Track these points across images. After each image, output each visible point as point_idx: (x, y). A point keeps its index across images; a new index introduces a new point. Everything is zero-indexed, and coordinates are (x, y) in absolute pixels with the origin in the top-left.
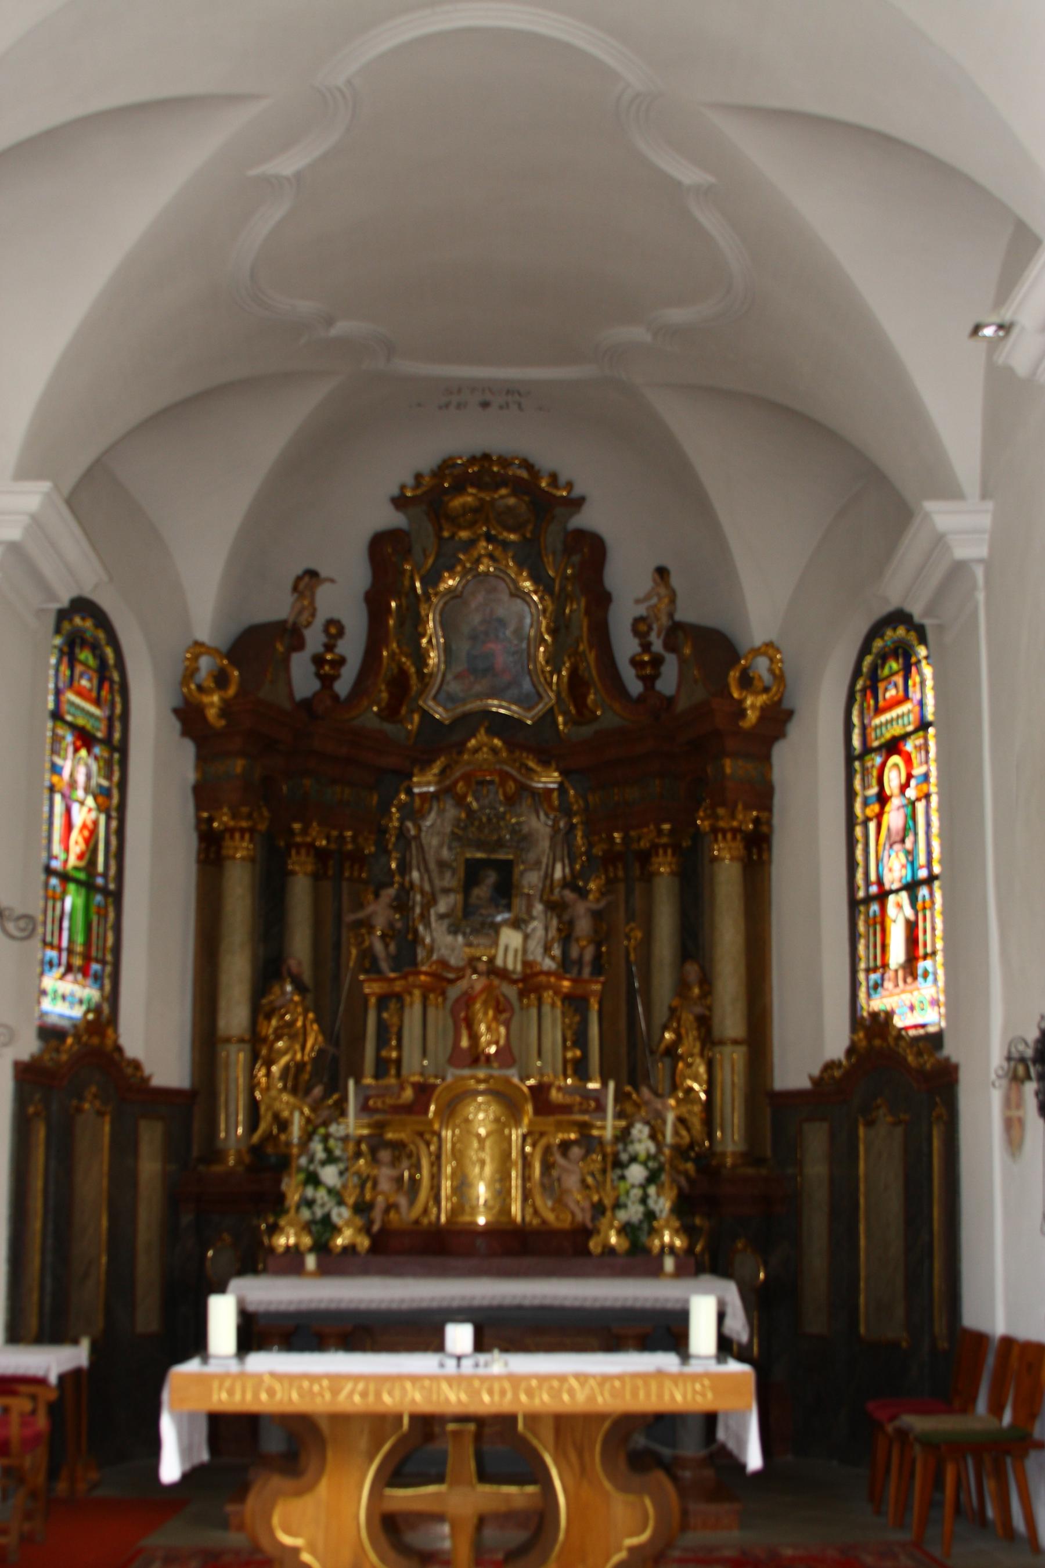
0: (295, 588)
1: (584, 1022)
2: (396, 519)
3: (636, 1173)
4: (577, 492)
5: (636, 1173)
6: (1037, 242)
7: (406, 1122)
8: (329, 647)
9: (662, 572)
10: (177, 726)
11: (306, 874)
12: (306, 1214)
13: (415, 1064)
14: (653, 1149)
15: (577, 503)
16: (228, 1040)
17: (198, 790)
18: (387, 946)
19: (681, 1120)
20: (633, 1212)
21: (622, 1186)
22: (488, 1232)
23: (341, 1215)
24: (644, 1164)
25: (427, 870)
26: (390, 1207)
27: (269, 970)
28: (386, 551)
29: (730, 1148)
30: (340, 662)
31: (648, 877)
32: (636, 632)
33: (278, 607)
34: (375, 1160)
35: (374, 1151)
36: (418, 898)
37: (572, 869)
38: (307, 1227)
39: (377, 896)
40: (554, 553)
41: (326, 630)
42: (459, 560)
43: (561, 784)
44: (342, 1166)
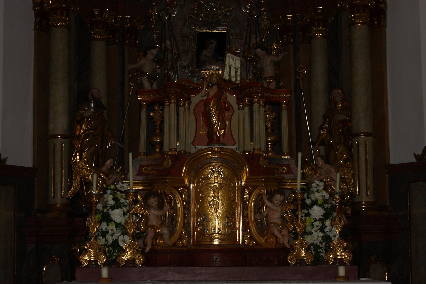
3: (317, 212)
5: (317, 212)
7: (167, 176)
12: (102, 241)
13: (171, 143)
14: (327, 196)
16: (55, 137)
18: (152, 84)
19: (343, 180)
20: (316, 237)
23: (124, 241)
26: (158, 235)
27: (80, 96)
29: (364, 199)
34: (146, 206)
35: (145, 199)
36: (170, 56)
38: (101, 249)
39: (145, 55)
42: (130, 250)
44: (125, 209)
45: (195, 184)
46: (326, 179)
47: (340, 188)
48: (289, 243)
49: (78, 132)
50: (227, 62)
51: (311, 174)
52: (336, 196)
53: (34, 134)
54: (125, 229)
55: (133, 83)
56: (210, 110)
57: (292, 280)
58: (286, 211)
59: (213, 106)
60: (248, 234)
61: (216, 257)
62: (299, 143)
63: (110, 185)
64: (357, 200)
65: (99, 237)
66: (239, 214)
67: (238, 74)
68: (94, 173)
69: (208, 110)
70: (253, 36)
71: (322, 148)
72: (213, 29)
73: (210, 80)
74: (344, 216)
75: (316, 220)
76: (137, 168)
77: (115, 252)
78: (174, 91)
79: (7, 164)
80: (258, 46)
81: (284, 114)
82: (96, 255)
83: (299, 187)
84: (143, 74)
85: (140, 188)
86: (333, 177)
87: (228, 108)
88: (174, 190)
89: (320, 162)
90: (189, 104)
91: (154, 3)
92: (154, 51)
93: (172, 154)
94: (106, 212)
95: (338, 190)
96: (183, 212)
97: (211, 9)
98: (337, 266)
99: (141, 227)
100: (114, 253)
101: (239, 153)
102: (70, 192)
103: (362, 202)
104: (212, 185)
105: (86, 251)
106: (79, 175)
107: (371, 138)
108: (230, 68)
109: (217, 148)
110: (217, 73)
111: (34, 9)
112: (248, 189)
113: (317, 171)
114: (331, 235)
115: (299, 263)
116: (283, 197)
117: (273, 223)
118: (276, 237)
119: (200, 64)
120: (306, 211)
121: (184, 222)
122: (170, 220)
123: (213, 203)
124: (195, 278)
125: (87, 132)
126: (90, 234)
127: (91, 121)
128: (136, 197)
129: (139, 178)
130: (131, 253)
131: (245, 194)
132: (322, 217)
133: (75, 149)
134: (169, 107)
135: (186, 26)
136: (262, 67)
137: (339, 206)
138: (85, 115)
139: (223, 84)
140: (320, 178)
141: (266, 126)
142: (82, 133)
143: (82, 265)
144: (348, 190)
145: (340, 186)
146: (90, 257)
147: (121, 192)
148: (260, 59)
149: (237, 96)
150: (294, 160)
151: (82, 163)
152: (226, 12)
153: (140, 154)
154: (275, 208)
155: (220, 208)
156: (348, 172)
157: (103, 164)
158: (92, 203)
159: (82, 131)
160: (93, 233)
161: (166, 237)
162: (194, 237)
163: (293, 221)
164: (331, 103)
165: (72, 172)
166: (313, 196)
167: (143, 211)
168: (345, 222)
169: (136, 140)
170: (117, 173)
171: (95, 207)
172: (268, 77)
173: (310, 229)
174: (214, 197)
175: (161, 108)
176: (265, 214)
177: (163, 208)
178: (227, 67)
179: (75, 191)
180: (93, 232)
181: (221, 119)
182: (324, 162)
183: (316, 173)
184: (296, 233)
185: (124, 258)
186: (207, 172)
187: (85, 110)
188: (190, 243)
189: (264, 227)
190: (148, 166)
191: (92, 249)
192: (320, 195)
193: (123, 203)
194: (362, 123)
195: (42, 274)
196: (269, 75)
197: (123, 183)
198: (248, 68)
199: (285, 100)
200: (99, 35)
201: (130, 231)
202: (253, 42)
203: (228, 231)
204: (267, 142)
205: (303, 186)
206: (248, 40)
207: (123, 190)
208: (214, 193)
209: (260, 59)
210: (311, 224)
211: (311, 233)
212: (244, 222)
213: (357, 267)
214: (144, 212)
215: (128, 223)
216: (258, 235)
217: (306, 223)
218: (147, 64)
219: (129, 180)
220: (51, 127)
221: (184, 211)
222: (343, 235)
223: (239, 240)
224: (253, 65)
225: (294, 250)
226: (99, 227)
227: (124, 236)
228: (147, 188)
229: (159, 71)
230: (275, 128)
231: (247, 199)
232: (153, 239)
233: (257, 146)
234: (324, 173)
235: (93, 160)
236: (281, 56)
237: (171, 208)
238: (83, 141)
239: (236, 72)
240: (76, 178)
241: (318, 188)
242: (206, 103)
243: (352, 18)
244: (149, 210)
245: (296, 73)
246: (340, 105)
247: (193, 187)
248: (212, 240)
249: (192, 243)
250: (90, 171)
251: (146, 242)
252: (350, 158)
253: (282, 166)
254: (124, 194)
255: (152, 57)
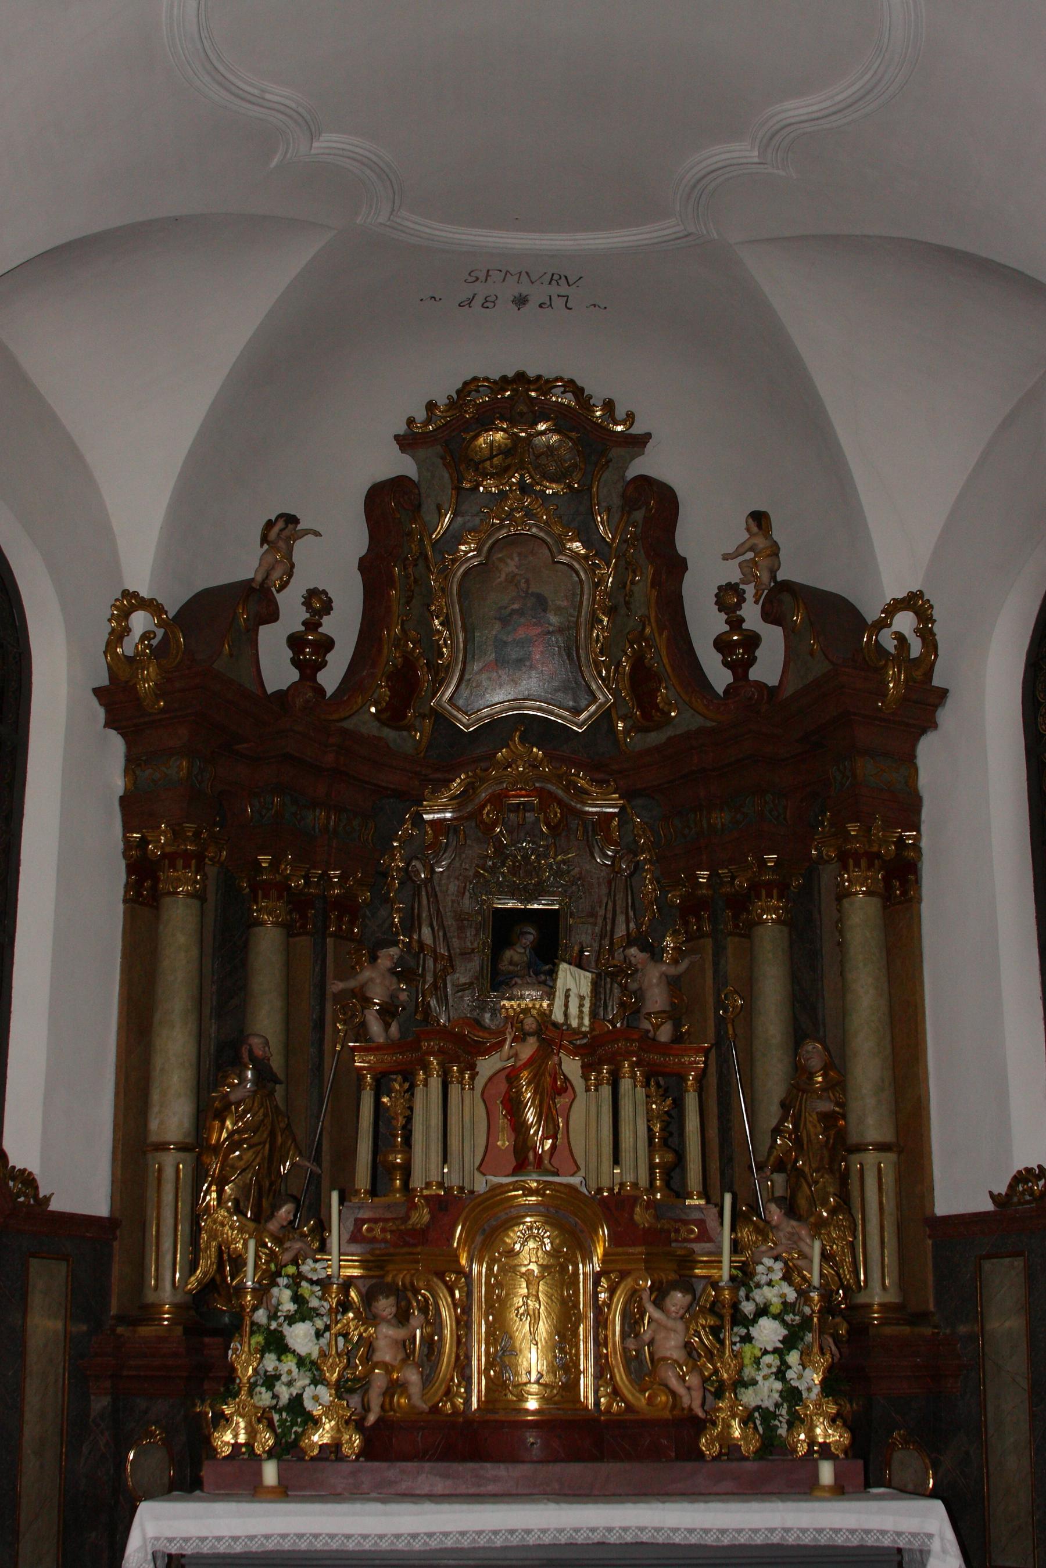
0: (264, 539)
1: (679, 1104)
2: (406, 466)
3: (768, 1332)
4: (637, 429)
5: (768, 1332)
6: (920, 594)
7: (420, 1248)
8: (312, 625)
9: (759, 519)
10: (101, 713)
11: (275, 924)
12: (264, 1398)
13: (427, 1169)
14: (791, 1295)
15: (639, 442)
16: (162, 1147)
17: (126, 802)
18: (387, 1026)
19: (825, 1257)
20: (766, 1392)
21: (749, 1352)
22: (544, 1423)
23: (318, 1399)
24: (778, 1317)
25: (442, 926)
26: (395, 1387)
27: (222, 1052)
28: (389, 506)
30: (327, 645)
31: (748, 929)
32: (721, 604)
33: (244, 563)
34: (369, 1317)
35: (368, 1298)
36: (430, 963)
37: (639, 926)
38: (264, 1417)
39: (373, 959)
40: (608, 510)
41: (307, 603)
42: (330, 1421)
43: (622, 809)
44: (320, 1324)
45: (485, 1265)
46: (790, 1254)
47: (822, 1275)
48: (703, 1405)
49: (215, 1136)
50: (560, 983)
51: (755, 1243)
52: (812, 1294)
53: (114, 1140)
54: (319, 1369)
55: (344, 1024)
56: (519, 1093)
57: (710, 1494)
58: (696, 1331)
59: (528, 1084)
60: (607, 1384)
61: (531, 1440)
62: (726, 1169)
63: (285, 1266)
64: (861, 1299)
65: (258, 1389)
66: (586, 1337)
67: (586, 1009)
68: (250, 1237)
69: (516, 1092)
70: (621, 919)
71: (779, 1178)
72: (529, 902)
73: (522, 1022)
74: (830, 1340)
75: (765, 1352)
76: (350, 1225)
77: (294, 1423)
78: (436, 1048)
79: (50, 1208)
80: (630, 941)
81: (691, 1101)
82: (251, 1433)
83: (726, 1276)
84: (367, 1002)
85: (356, 1272)
86: (806, 1249)
87: (565, 1087)
88: (435, 1279)
89: (775, 1214)
90: (472, 1078)
91: (396, 841)
92: (394, 951)
93: (431, 1196)
94: (275, 1330)
95: (816, 1281)
96: (455, 1332)
97: (526, 858)
98: (816, 1460)
99: (357, 1366)
100: (292, 1426)
101: (587, 1193)
102: (193, 1279)
103: (873, 1305)
104: (523, 1269)
105: (227, 1420)
106: (215, 1240)
107: (892, 1156)
108: (567, 997)
109: (537, 1181)
110: (537, 1006)
111: (125, 855)
112: (608, 1279)
113: (768, 1235)
114: (802, 1387)
115: (725, 1454)
116: (689, 1297)
117: (664, 1359)
118: (673, 1393)
119: (498, 980)
120: (743, 1331)
121: (458, 1357)
122: (426, 1350)
123: (527, 1312)
124: (482, 1490)
125: (236, 1137)
126: (238, 1381)
127: (245, 1112)
128: (347, 1294)
129: (354, 1248)
130: (332, 1428)
131: (599, 1289)
132: (781, 1346)
133: (207, 1176)
134: (426, 1085)
135: (467, 893)
136: (640, 988)
137: (819, 1320)
138: (233, 1098)
139: (550, 1035)
140: (775, 1252)
141: (650, 1130)
142: (225, 1140)
143: (218, 1453)
144: (840, 1279)
145: (821, 1271)
146: (236, 1436)
147: (312, 1282)
148: (637, 970)
149: (582, 1059)
150: (715, 1211)
151: (223, 1212)
152: (558, 863)
153: (357, 1192)
154: (670, 1323)
155: (541, 1323)
156: (839, 1237)
157: (272, 1216)
158: (243, 1307)
159: (224, 1135)
160: (245, 1380)
161: (415, 1389)
162: (480, 1391)
163: (711, 1353)
164: (800, 1073)
165: (200, 1233)
166: (759, 1296)
167: (362, 1329)
168: (833, 1355)
169: (347, 1155)
170: (303, 1235)
171: (251, 1317)
172: (654, 1013)
173: (753, 1373)
174: (527, 1297)
175: (406, 1085)
176: (647, 1337)
177: (408, 1320)
178: (560, 995)
179: (205, 1276)
180: (244, 1376)
181: (546, 1115)
182: (785, 1214)
183: (765, 1240)
184: (721, 1382)
185: (315, 1438)
186: (512, 1238)
187: (232, 1086)
188: (471, 1405)
189: (643, 1368)
190: (375, 1221)
191: (242, 1416)
192: (775, 1292)
193: (315, 1309)
194: (870, 1120)
195: (126, 1469)
196: (657, 1007)
197: (316, 1261)
198: (608, 992)
199: (694, 1069)
200: (269, 914)
201: (332, 1375)
202: (621, 931)
203: (561, 1378)
204: (652, 1167)
205: (734, 1272)
206: (608, 928)
207: (315, 1278)
208: (527, 1287)
209: (637, 970)
210: (755, 1362)
211: (754, 1383)
212: (598, 1356)
213: (861, 1462)
214: (365, 1331)
215: (325, 1356)
216: (630, 1386)
217: (742, 1358)
218: (378, 981)
219: (330, 1254)
220: (154, 1125)
221: (458, 1329)
222: (828, 1387)
223: (586, 1398)
224: (620, 985)
225: (714, 1424)
226: (258, 1365)
227: (316, 1386)
228: (372, 1273)
229: (403, 997)
230: (669, 1136)
231: (604, 1302)
232: (384, 1394)
233: (629, 1179)
234: (784, 1241)
235: (249, 1200)
236: (684, 965)
237: (428, 1323)
238: (226, 1156)
239: (581, 1006)
240: (208, 1247)
241: (770, 1276)
242: (512, 1076)
243: (843, 880)
244: (375, 1326)
245: (719, 1004)
246: (820, 1079)
247: (480, 1273)
248: (522, 1399)
249: (475, 1406)
250: (241, 1230)
251: (368, 1402)
252: (845, 1202)
253: (686, 1223)
254: (319, 1288)
255: (389, 964)
